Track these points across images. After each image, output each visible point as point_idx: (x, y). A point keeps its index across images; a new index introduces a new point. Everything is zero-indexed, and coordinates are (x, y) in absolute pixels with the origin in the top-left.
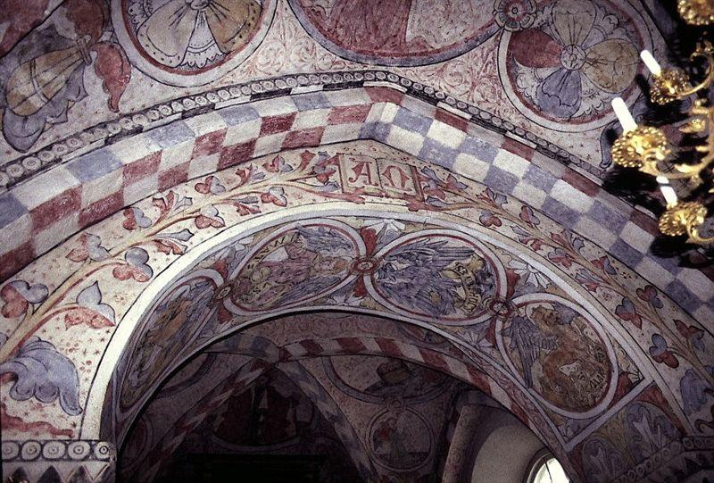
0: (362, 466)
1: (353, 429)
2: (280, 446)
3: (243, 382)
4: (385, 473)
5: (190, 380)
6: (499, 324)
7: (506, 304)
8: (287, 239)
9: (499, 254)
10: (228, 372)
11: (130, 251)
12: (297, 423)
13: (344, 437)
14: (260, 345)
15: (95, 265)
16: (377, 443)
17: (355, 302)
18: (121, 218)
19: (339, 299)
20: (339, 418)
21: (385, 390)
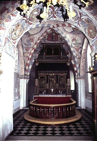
0: (70, 45)
1: (68, 39)
2: (57, 41)
3: (48, 32)
4: (74, 46)
5: (39, 32)
6: (80, 22)
7: (80, 18)
8: (36, 10)
9: (77, 9)
10: (45, 30)
11: (8, 17)
12: (60, 38)
13: (66, 40)
14: (48, 26)
15: (3, 20)
16: (73, 41)
17: (55, 19)
18: (6, 11)
19: (52, 19)
20: (65, 37)
21: (74, 32)
